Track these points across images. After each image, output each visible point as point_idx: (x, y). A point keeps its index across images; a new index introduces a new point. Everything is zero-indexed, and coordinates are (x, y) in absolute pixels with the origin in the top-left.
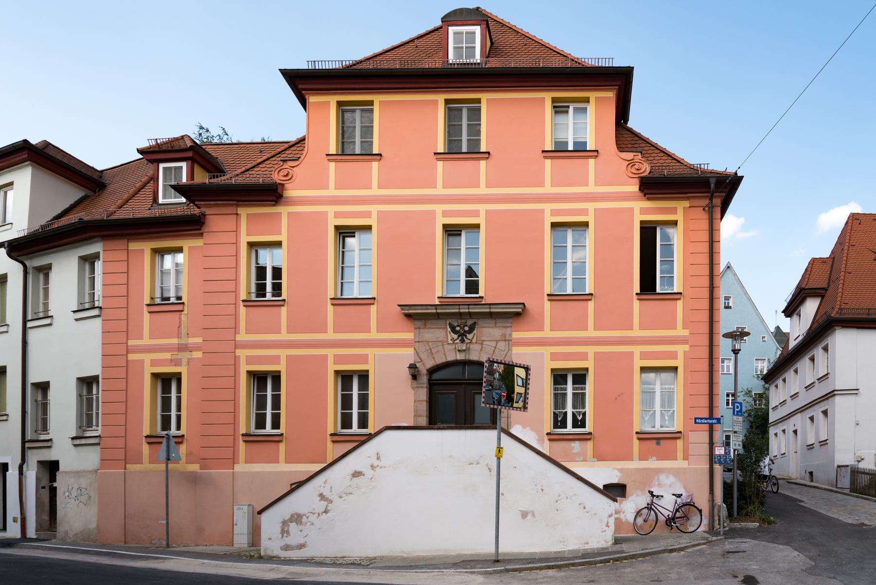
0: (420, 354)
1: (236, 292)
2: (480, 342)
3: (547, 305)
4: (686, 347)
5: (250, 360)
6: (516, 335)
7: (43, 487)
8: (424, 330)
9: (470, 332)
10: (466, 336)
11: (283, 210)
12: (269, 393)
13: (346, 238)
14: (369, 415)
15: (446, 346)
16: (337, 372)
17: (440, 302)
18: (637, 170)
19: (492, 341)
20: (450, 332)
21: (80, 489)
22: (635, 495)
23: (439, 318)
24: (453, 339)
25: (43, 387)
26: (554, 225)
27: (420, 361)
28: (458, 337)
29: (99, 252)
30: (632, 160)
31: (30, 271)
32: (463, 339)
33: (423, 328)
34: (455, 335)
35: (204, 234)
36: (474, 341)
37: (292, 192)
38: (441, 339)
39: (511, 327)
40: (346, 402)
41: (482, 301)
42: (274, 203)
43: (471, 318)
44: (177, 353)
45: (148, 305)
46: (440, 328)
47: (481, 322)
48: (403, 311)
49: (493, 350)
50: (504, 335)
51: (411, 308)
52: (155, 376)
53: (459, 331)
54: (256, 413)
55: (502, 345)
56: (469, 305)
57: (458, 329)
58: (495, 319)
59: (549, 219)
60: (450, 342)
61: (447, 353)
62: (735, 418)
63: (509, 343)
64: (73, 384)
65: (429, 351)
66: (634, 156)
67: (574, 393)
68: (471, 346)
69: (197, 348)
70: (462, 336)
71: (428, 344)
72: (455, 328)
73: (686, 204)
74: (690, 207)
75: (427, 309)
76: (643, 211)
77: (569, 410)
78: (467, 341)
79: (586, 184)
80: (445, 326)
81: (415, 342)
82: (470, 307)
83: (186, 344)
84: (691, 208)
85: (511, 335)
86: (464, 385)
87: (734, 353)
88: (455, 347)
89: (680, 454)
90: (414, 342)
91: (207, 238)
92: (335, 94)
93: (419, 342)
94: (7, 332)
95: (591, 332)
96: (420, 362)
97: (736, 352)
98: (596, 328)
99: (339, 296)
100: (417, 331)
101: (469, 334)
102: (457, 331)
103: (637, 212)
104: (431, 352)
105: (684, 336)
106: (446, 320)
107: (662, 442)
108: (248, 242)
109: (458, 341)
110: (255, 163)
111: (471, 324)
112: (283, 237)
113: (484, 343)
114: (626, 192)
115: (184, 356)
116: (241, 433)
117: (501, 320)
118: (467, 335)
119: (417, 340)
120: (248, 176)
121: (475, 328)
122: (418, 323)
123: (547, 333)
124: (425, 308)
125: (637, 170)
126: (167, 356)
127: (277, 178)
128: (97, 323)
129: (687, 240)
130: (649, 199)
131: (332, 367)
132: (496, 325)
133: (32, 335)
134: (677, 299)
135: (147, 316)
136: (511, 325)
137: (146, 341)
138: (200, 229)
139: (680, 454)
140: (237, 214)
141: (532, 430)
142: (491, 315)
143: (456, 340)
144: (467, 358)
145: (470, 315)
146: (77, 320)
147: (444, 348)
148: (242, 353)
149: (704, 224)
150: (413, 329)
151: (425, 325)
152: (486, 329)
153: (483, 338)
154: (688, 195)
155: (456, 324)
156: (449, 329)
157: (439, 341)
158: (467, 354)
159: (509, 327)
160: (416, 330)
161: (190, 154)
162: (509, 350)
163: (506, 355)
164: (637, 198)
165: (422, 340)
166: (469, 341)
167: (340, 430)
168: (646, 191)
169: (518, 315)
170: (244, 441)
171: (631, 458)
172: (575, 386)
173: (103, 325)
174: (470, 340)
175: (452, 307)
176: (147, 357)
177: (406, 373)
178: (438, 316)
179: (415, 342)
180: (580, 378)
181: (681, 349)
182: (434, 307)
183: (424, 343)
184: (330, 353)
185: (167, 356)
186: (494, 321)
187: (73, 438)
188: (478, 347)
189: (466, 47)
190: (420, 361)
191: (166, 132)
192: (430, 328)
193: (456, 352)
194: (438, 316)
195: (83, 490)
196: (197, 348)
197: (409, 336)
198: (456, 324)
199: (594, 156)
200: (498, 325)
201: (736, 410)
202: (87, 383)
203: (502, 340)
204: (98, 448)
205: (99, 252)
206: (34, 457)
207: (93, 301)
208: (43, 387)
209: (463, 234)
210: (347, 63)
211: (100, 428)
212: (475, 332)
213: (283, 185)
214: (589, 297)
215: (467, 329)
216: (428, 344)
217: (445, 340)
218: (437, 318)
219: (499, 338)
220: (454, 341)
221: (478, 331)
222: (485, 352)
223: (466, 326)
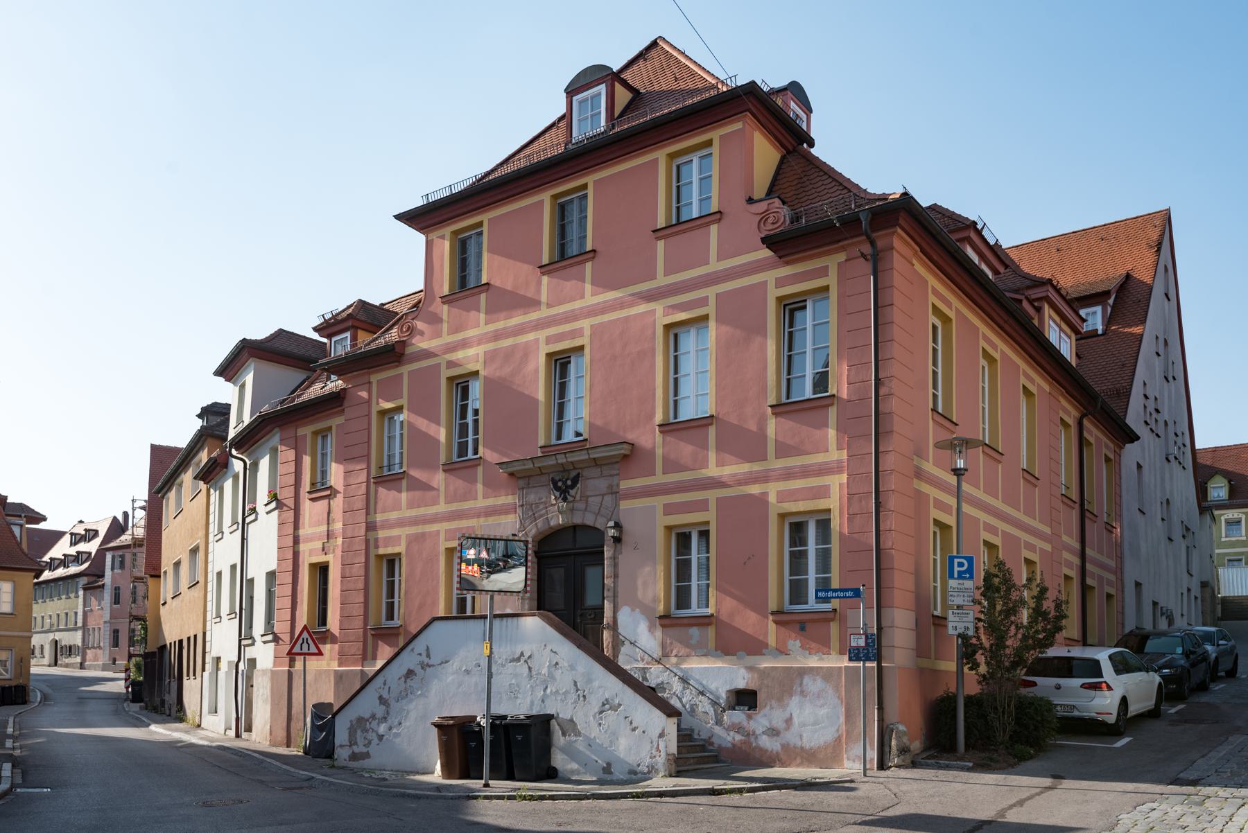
6: (625, 485)
9: (573, 487)
11: (405, 369)
13: (795, 312)
16: (669, 529)
17: (542, 453)
18: (773, 223)
19: (597, 496)
22: (768, 707)
25: (251, 581)
35: (346, 409)
36: (578, 498)
39: (618, 474)
40: (798, 561)
41: (586, 445)
42: (396, 364)
43: (575, 468)
50: (611, 486)
57: (560, 484)
66: (769, 204)
68: (576, 505)
73: (842, 257)
74: (846, 260)
78: (570, 498)
84: (848, 262)
85: (618, 485)
86: (573, 556)
92: (449, 225)
99: (784, 400)
101: (572, 489)
106: (601, 467)
113: (590, 499)
114: (744, 264)
116: (770, 612)
122: (522, 483)
125: (773, 223)
130: (788, 263)
134: (828, 406)
136: (618, 472)
138: (341, 405)
141: (642, 613)
152: (591, 480)
153: (589, 493)
154: (841, 244)
156: (552, 486)
159: (617, 475)
161: (349, 323)
164: (771, 265)
167: (787, 606)
168: (782, 253)
187: (262, 636)
191: (339, 302)
197: (508, 499)
198: (557, 478)
199: (716, 220)
201: (956, 569)
203: (609, 494)
209: (809, 304)
210: (480, 176)
212: (579, 485)
214: (709, 421)
215: (569, 483)
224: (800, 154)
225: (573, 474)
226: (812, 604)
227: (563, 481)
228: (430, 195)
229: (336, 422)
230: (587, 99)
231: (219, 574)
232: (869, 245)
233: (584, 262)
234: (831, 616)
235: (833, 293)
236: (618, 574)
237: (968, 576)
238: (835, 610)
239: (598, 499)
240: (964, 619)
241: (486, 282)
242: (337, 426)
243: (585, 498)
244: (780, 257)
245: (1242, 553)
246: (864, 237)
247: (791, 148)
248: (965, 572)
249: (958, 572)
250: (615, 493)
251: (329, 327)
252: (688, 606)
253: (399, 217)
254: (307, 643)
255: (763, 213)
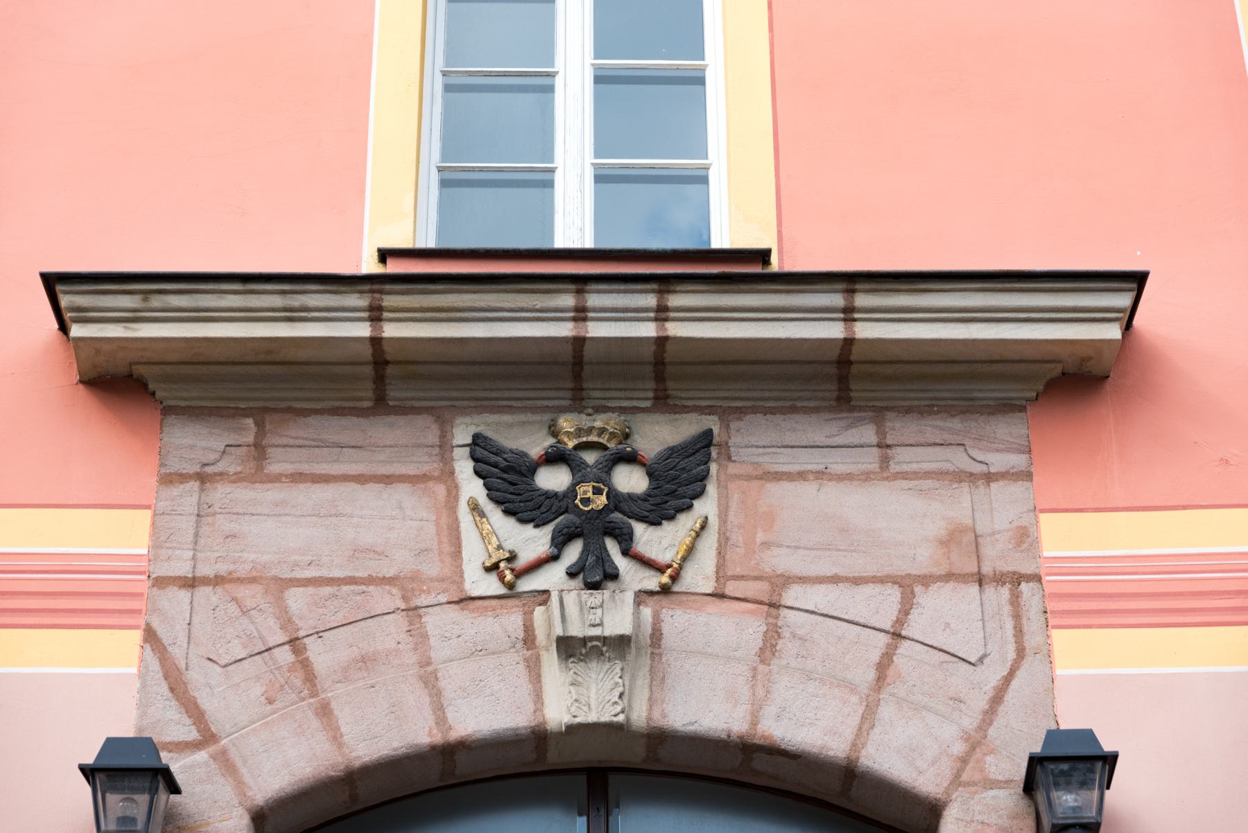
0: (198, 677)
8: (243, 494)
14: (82, 763)
15: (442, 621)
19: (857, 581)
20: (475, 508)
23: (381, 405)
27: (193, 734)
28: (561, 541)
32: (603, 559)
33: (238, 479)
34: (529, 530)
36: (699, 576)
38: (399, 562)
39: (1027, 476)
43: (663, 403)
46: (388, 480)
49: (875, 656)
51: (156, 301)
53: (571, 492)
57: (553, 479)
58: (878, 413)
60: (491, 586)
61: (452, 678)
63: (1015, 600)
65: (285, 656)
68: (676, 620)
71: (280, 603)
72: (533, 469)
75: (292, 313)
80: (429, 465)
81: (161, 582)
82: (675, 300)
85: (1025, 538)
88: (529, 629)
90: (141, 585)
93: (191, 583)
96: (196, 746)
100: (187, 497)
102: (550, 496)
104: (305, 665)
109: (553, 577)
111: (672, 451)
117: (932, 428)
118: (639, 528)
119: (182, 568)
121: (704, 477)
124: (277, 301)
132: (885, 461)
136: (1017, 461)
143: (536, 566)
144: (639, 716)
150: (153, 481)
151: (259, 450)
152: (807, 489)
153: (782, 561)
156: (472, 487)
157: (370, 580)
158: (642, 683)
160: (176, 490)
162: (1021, 653)
163: (997, 698)
165: (222, 568)
166: (652, 581)
174: (660, 569)
179: (161, 582)
183: (244, 592)
186: (868, 434)
190: (193, 734)
192: (298, 478)
193: (534, 669)
198: (536, 445)
200: (905, 459)
203: (949, 577)
212: (706, 507)
216: (280, 603)
217: (432, 568)
219: (923, 559)
220: (519, 574)
221: (735, 499)
222: (809, 676)
223: (631, 458)
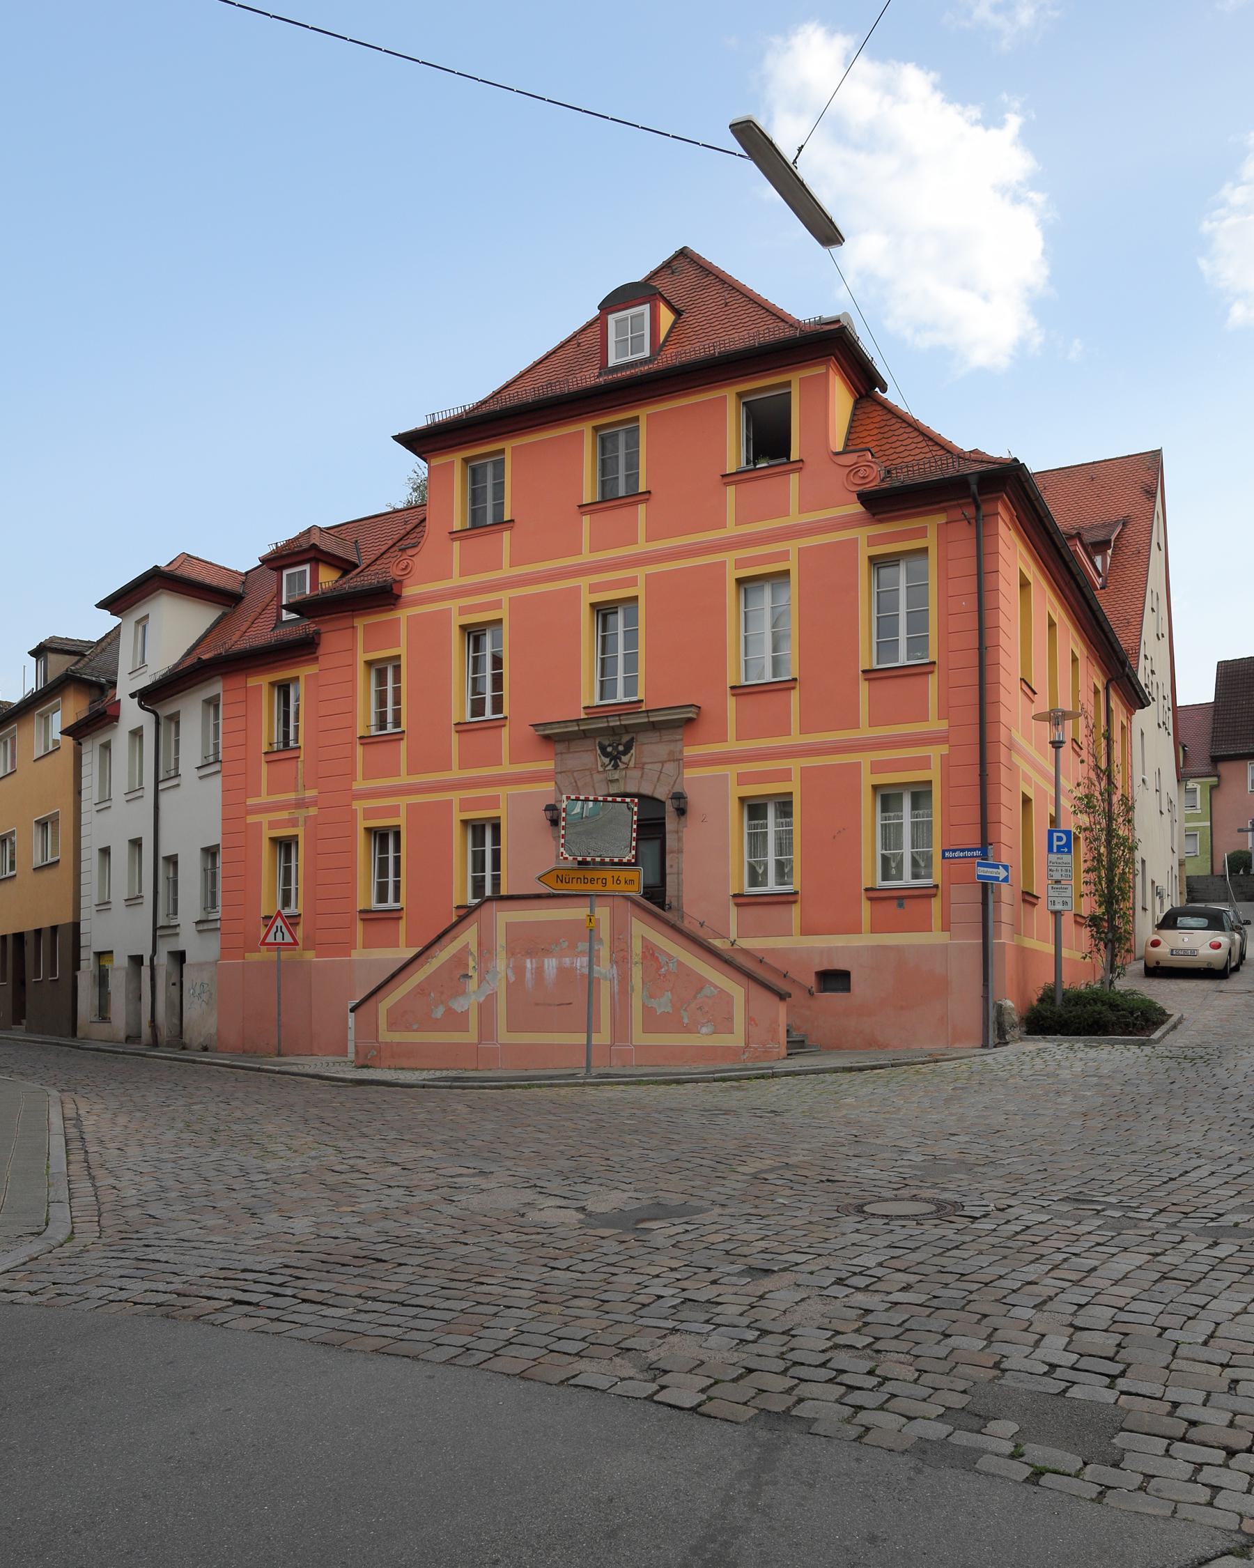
1: (352, 727)
2: (641, 765)
3: (731, 702)
4: (944, 749)
5: (369, 813)
6: (690, 751)
7: (174, 984)
9: (625, 752)
10: (620, 759)
12: (391, 855)
18: (864, 478)
21: (202, 985)
24: (603, 765)
25: (172, 861)
26: (740, 582)
28: (611, 761)
29: (219, 694)
30: (855, 464)
31: (162, 721)
36: (632, 764)
37: (409, 591)
39: (682, 740)
43: (627, 732)
44: (680, 737)
45: (266, 753)
46: (587, 751)
47: (642, 738)
48: (537, 733)
50: (671, 753)
52: (274, 841)
54: (378, 883)
55: (670, 768)
56: (619, 715)
57: (609, 749)
59: (732, 574)
60: (601, 769)
62: (1053, 857)
64: (198, 853)
66: (859, 456)
67: (886, 824)
69: (314, 803)
70: (615, 758)
73: (941, 518)
74: (947, 523)
75: (566, 727)
76: (872, 541)
77: (907, 851)
79: (786, 513)
81: (556, 773)
83: (303, 799)
85: (681, 752)
87: (1053, 747)
89: (936, 921)
91: (324, 661)
92: (459, 450)
93: (560, 773)
94: (142, 797)
95: (796, 738)
97: (1057, 745)
98: (739, 738)
103: (862, 543)
104: (577, 785)
105: (941, 731)
107: (905, 902)
108: (365, 662)
110: (378, 553)
112: (402, 650)
115: (301, 814)
119: (559, 770)
120: (362, 578)
122: (560, 747)
123: (732, 745)
126: (284, 815)
127: (395, 572)
128: (218, 780)
129: (944, 577)
130: (880, 521)
131: (458, 816)
133: (163, 798)
135: (264, 767)
137: (265, 798)
138: (315, 653)
139: (936, 921)
140: (353, 627)
142: (654, 727)
145: (627, 728)
146: (201, 778)
147: (592, 777)
148: (359, 805)
149: (969, 548)
151: (569, 748)
153: (644, 760)
155: (607, 743)
156: (599, 752)
161: (312, 554)
163: (675, 782)
169: (690, 721)
170: (361, 919)
171: (856, 929)
172: (753, 822)
173: (223, 782)
175: (600, 720)
176: (264, 819)
177: (542, 818)
178: (585, 735)
179: (556, 773)
180: (785, 807)
181: (936, 753)
182: (575, 723)
184: (455, 796)
185: (284, 815)
186: (658, 734)
187: (198, 923)
188: (637, 773)
189: (632, 338)
191: (286, 531)
194: (585, 735)
195: (205, 986)
196: (314, 803)
197: (549, 765)
198: (607, 743)
200: (665, 738)
201: (1056, 843)
202: (210, 853)
203: (669, 761)
204: (218, 934)
205: (219, 694)
206: (165, 947)
207: (216, 753)
208: (172, 861)
211: (219, 908)
212: (633, 751)
213: (401, 582)
215: (621, 748)
217: (594, 767)
218: (583, 736)
224: (875, 401)
225: (625, 739)
226: (907, 880)
227: (613, 747)
228: (436, 415)
229: (304, 672)
230: (627, 318)
231: (105, 852)
232: (974, 508)
233: (637, 503)
234: (933, 891)
235: (933, 553)
236: (204, 861)
237: (1066, 850)
238: (936, 886)
239: (657, 767)
240: (1063, 894)
241: (509, 519)
242: (306, 676)
243: (641, 766)
244: (874, 515)
245: (1196, 828)
246: (970, 500)
247: (863, 391)
248: (1063, 846)
249: (1057, 846)
250: (680, 762)
251: (278, 560)
252: (386, 901)
253: (396, 438)
254: (281, 931)
255: (850, 466)
